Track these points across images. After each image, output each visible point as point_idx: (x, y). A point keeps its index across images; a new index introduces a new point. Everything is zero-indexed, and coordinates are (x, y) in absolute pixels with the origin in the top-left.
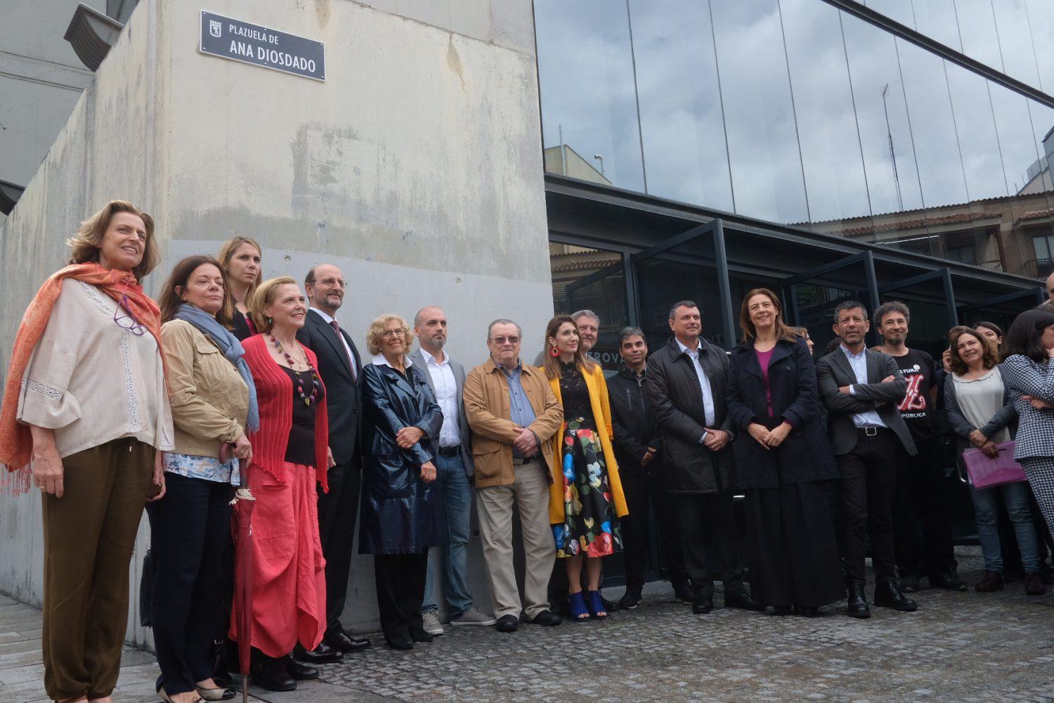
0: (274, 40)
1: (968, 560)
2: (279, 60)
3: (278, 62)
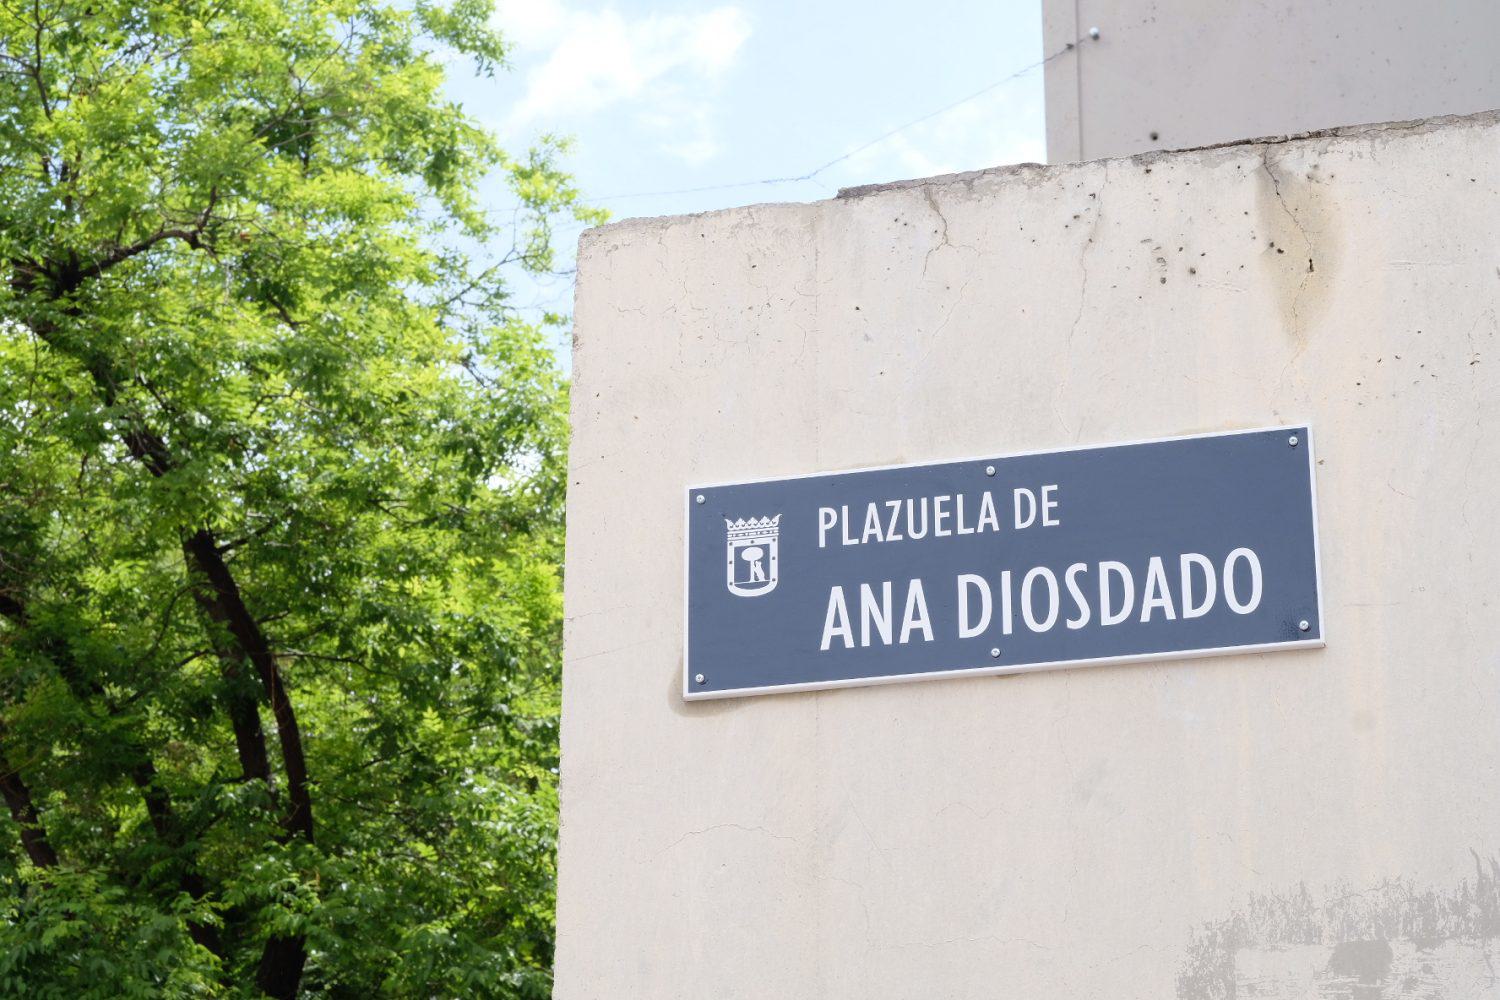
0: (1037, 507)
1: (271, 533)
2: (1069, 609)
3: (1061, 621)
